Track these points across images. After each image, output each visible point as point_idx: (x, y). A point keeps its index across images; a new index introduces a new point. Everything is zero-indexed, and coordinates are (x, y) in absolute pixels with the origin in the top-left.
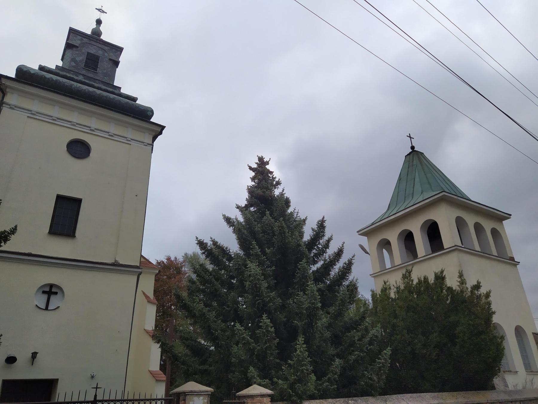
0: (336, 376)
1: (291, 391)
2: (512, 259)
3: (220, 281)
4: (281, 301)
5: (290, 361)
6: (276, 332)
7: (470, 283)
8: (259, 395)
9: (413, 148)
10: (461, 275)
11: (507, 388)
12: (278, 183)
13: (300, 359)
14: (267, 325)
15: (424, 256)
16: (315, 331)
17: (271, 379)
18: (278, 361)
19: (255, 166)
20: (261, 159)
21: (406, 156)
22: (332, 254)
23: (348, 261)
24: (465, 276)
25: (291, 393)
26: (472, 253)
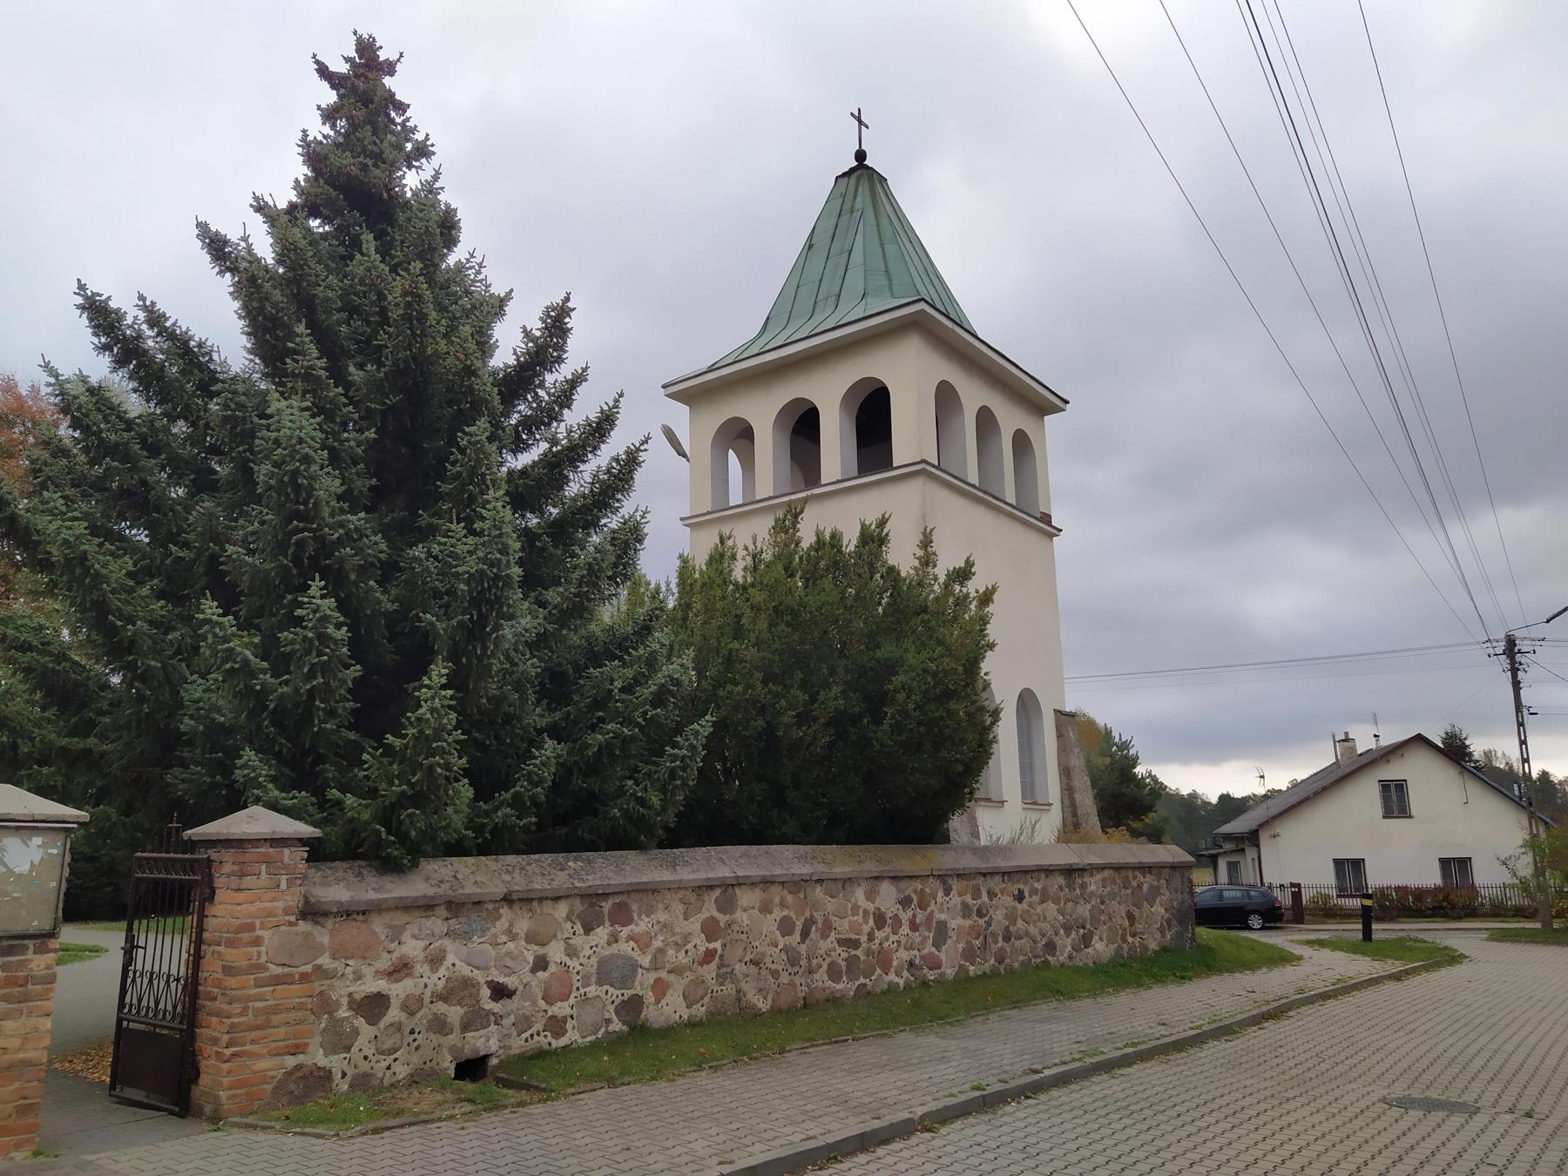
0: (539, 789)
1: (383, 829)
2: (1046, 519)
3: (163, 456)
4: (383, 546)
5: (390, 738)
6: (354, 643)
7: (947, 561)
8: (265, 840)
9: (861, 156)
10: (926, 542)
11: (975, 840)
12: (423, 151)
13: (427, 732)
14: (325, 619)
15: (838, 482)
16: (489, 653)
17: (319, 792)
18: (352, 736)
19: (341, 68)
20: (366, 47)
21: (839, 179)
22: (578, 425)
23: (627, 453)
24: (936, 546)
25: (384, 837)
26: (959, 487)
